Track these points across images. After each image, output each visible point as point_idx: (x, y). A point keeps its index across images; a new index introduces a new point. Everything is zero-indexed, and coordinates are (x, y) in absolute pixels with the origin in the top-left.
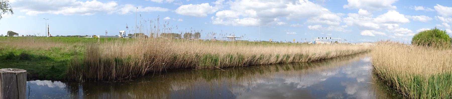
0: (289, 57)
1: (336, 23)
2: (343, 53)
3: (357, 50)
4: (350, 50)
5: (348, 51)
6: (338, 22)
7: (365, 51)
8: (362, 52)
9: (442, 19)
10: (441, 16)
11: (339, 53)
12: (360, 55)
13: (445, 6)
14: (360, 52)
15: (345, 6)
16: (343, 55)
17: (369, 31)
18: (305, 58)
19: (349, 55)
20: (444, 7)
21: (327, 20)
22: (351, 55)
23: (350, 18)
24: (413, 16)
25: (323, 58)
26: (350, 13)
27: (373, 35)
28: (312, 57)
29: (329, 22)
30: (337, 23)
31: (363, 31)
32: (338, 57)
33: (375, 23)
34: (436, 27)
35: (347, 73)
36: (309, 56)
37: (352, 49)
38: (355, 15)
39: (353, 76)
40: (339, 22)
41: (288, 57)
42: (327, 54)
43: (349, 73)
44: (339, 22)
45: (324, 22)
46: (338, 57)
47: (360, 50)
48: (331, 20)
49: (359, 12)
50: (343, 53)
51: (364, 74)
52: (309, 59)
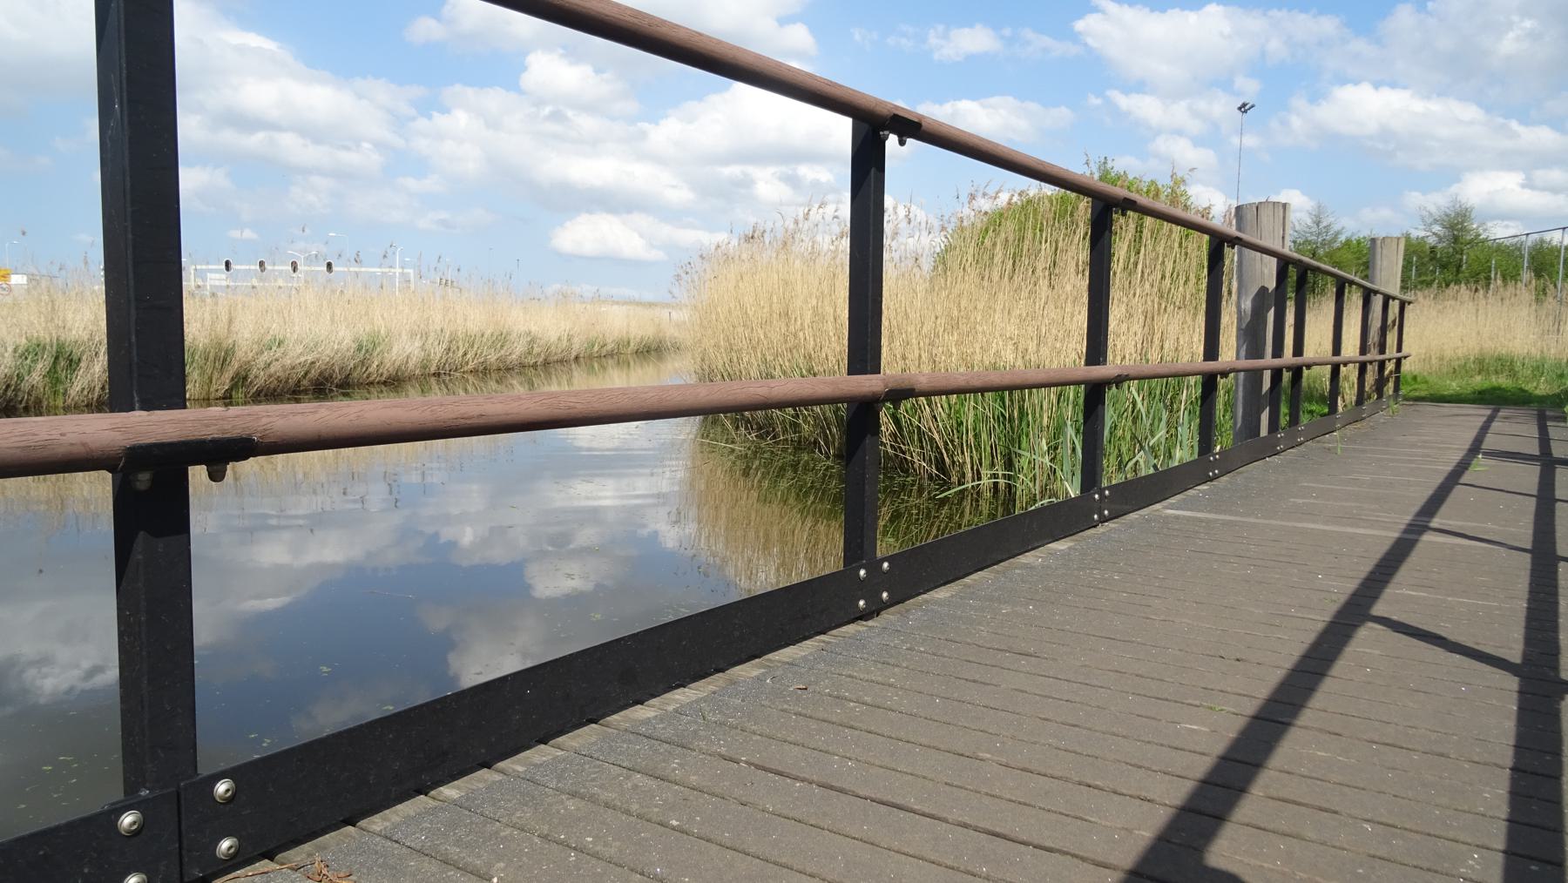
0: (73, 363)
1: (350, 158)
2: (465, 354)
3: (559, 339)
4: (509, 334)
5: (502, 339)
6: (366, 145)
7: (609, 347)
8: (591, 357)
9: (1146, 107)
10: (1140, 87)
11: (437, 353)
12: (575, 374)
13: (1163, 11)
14: (577, 358)
15: (425, 29)
16: (471, 366)
17: (610, 217)
18: (202, 373)
19: (508, 369)
20: (1157, 14)
21: (273, 127)
22: (523, 366)
23: (461, 119)
24: (959, 99)
25: (338, 377)
26: (458, 88)
27: (657, 255)
28: (265, 357)
29: (290, 146)
30: (364, 158)
31: (568, 224)
32: (437, 375)
33: (658, 160)
34: (1109, 165)
35: (447, 534)
36: (240, 354)
37: (522, 328)
38: (494, 99)
39: (499, 555)
40: (379, 145)
41: (62, 363)
42: (366, 349)
43: (467, 536)
44: (379, 145)
45: (255, 141)
46: (433, 380)
47: (576, 340)
48: (312, 133)
49: (529, 80)
50: (465, 354)
51: (586, 536)
52: (237, 374)
